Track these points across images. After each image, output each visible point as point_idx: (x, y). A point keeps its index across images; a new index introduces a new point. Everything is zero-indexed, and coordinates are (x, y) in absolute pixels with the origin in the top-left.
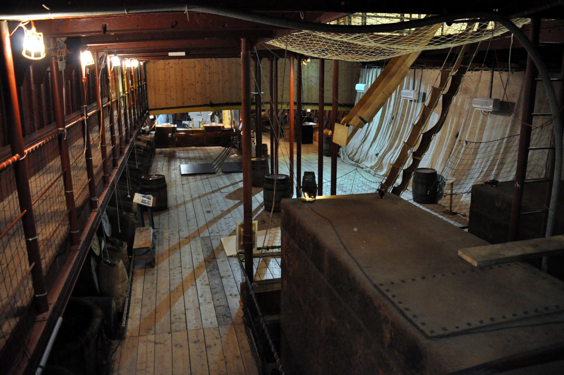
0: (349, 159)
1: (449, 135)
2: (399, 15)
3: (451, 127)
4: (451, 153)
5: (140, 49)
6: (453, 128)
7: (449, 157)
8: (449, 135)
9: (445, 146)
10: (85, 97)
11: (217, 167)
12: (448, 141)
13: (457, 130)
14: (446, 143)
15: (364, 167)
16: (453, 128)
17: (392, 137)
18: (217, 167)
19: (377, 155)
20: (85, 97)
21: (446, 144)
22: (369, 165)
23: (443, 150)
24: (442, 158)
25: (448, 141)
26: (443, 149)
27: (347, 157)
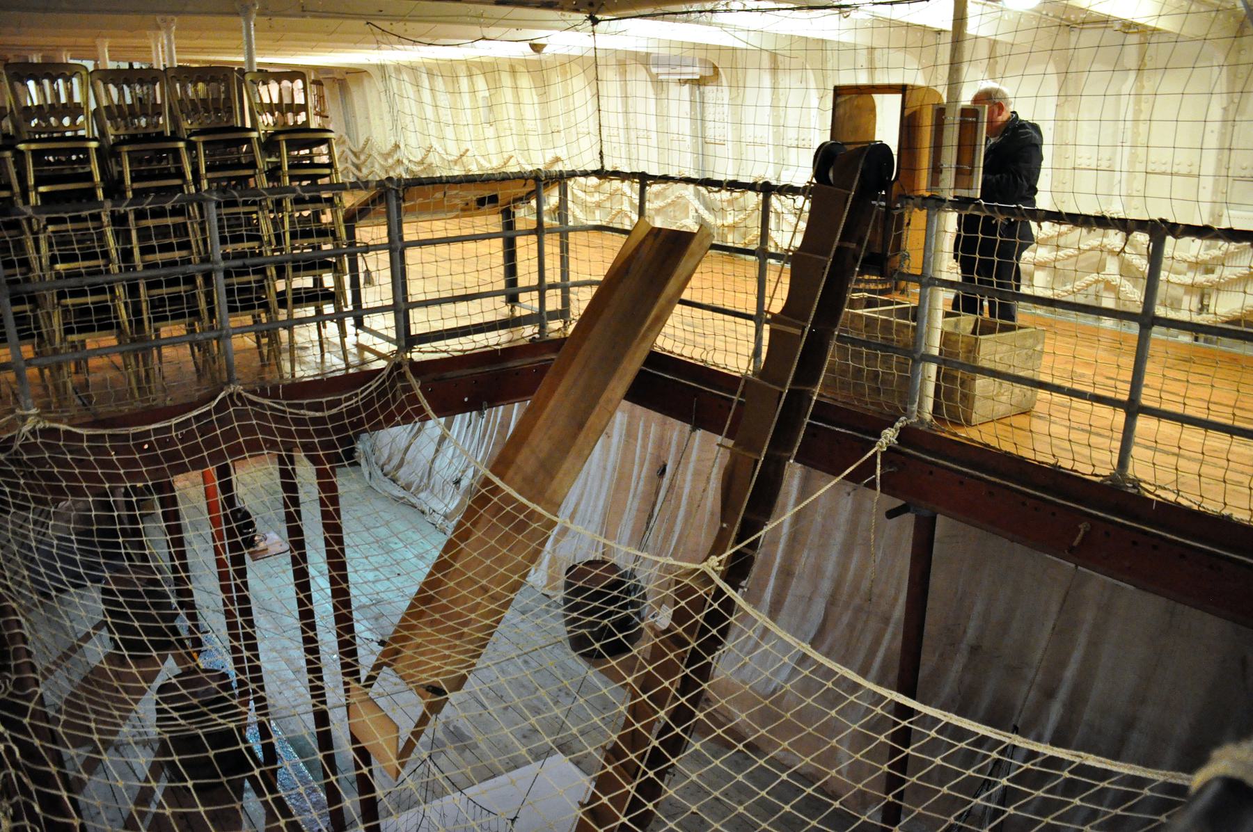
0: (385, 475)
1: (642, 466)
2: (918, 218)
3: (644, 447)
4: (651, 516)
5: (866, 295)
6: (650, 449)
7: (647, 527)
8: (642, 466)
9: (634, 496)
10: (998, 480)
11: (1029, 692)
12: (641, 483)
13: (659, 457)
14: (636, 489)
15: (427, 511)
16: (650, 449)
17: (491, 437)
18: (1029, 692)
19: (457, 482)
20: (998, 480)
21: (635, 492)
22: (440, 507)
23: (628, 507)
24: (630, 525)
25: (641, 483)
26: (629, 502)
27: (379, 472)
